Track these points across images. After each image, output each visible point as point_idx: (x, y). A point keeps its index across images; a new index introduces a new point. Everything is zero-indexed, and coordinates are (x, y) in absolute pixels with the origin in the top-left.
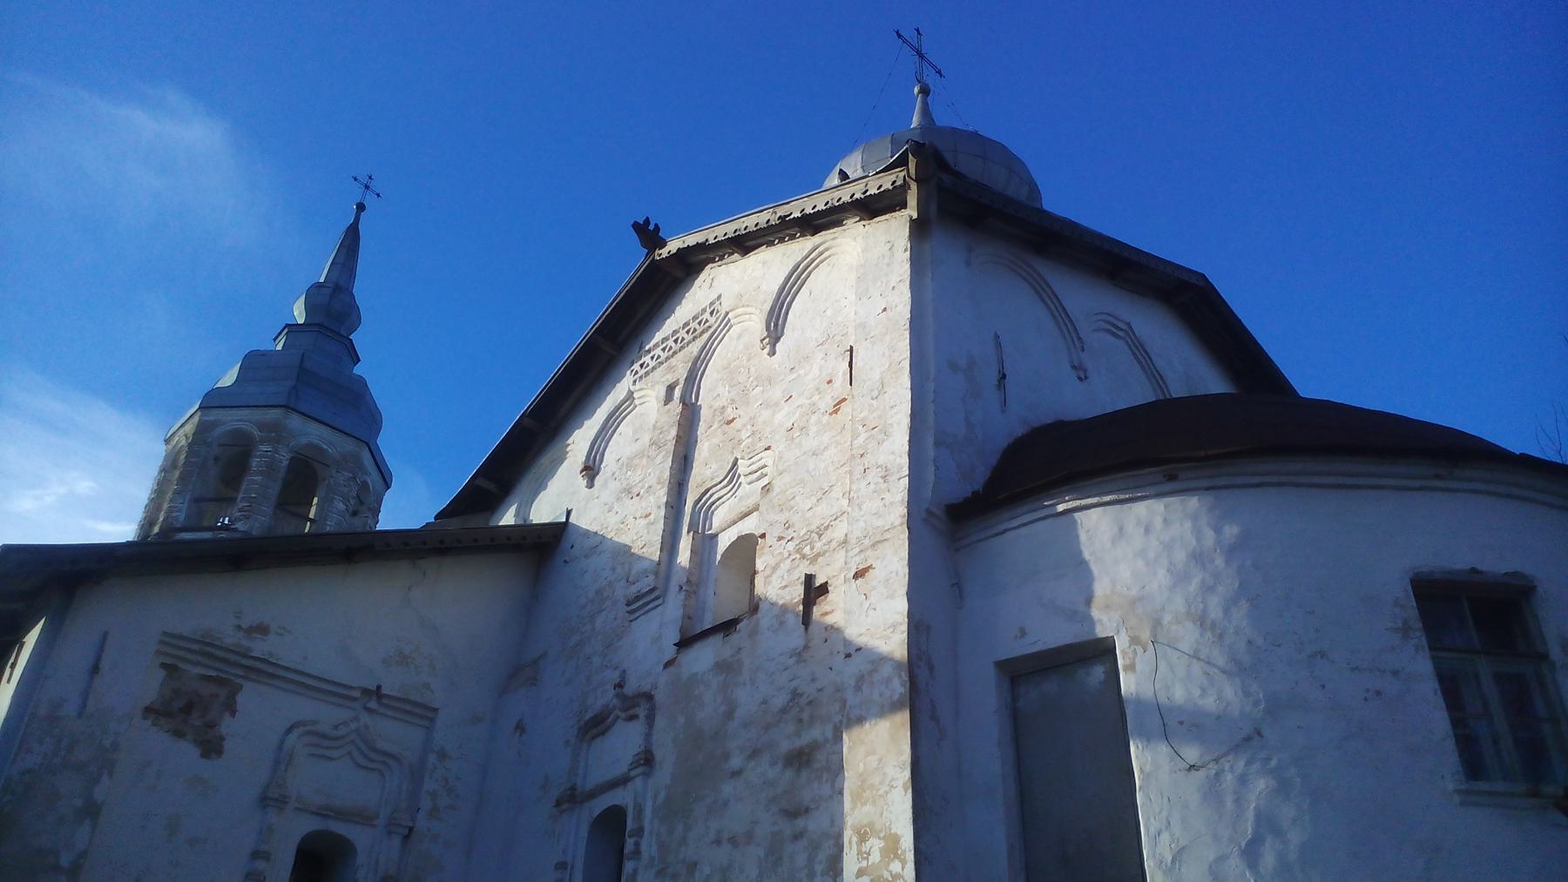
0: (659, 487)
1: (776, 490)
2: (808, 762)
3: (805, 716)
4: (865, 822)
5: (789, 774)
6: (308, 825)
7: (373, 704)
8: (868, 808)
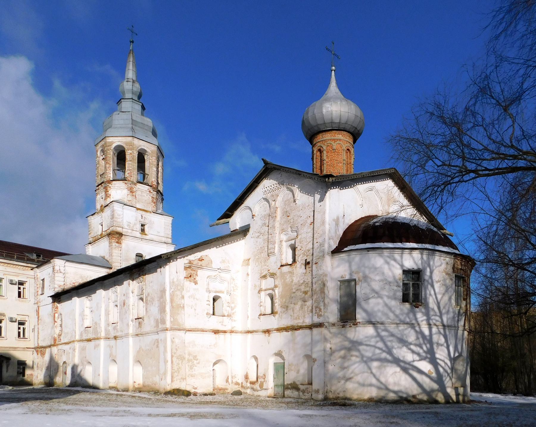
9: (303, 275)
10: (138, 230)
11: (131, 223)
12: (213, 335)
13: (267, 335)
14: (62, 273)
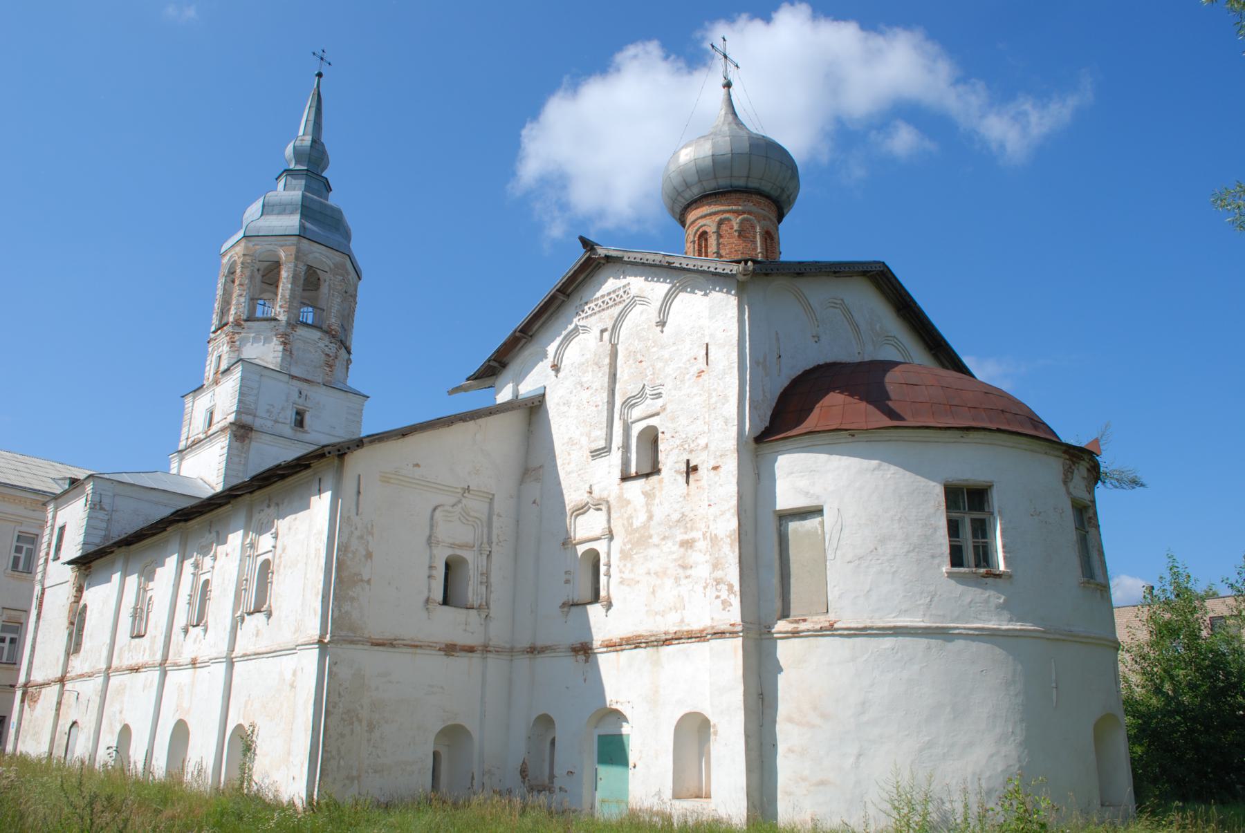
0: (602, 391)
1: (668, 410)
4: (719, 577)
5: (682, 550)
6: (448, 552)
8: (720, 572)
9: (681, 499)
10: (288, 421)
11: (274, 407)
12: (441, 660)
13: (581, 657)
14: (105, 510)
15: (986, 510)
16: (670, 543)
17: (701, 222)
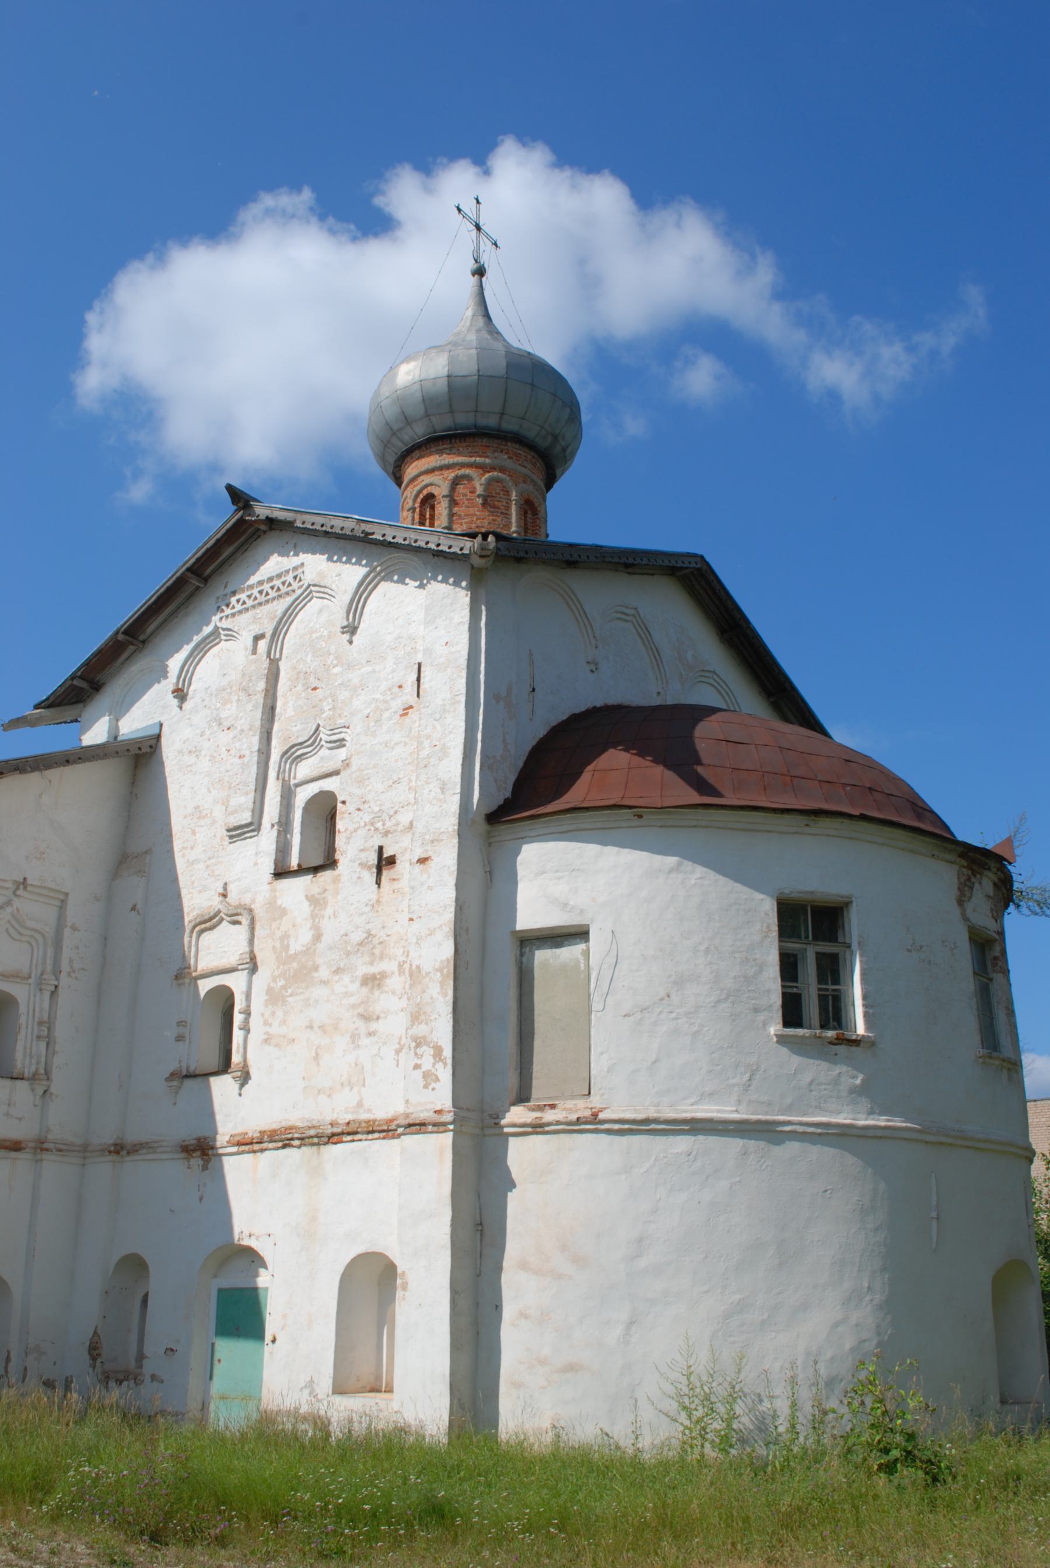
1: (354, 766)
2: (379, 986)
3: (377, 951)
5: (365, 990)
7: (20, 892)
8: (423, 1027)
15: (840, 940)
16: (346, 979)
17: (427, 479)
